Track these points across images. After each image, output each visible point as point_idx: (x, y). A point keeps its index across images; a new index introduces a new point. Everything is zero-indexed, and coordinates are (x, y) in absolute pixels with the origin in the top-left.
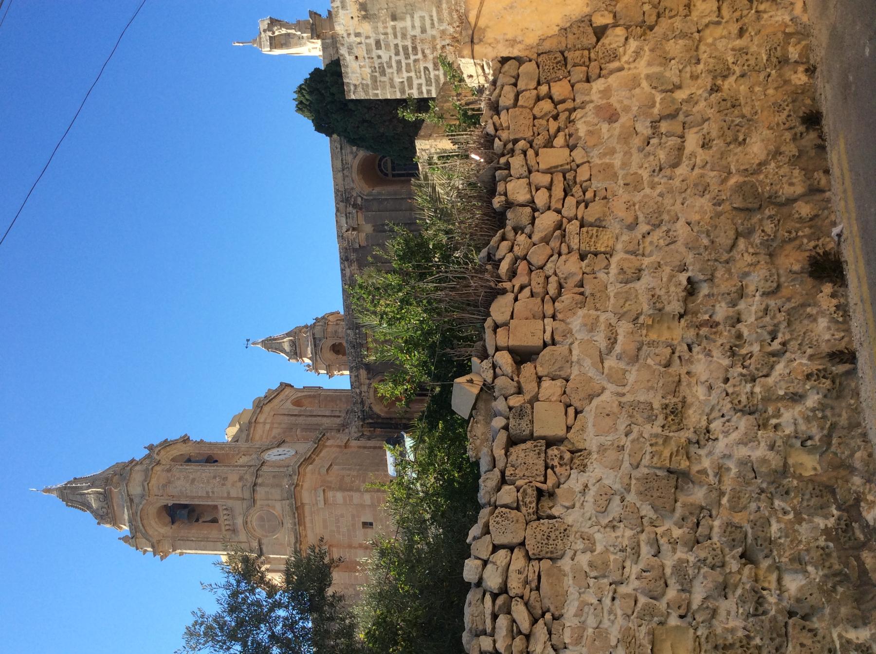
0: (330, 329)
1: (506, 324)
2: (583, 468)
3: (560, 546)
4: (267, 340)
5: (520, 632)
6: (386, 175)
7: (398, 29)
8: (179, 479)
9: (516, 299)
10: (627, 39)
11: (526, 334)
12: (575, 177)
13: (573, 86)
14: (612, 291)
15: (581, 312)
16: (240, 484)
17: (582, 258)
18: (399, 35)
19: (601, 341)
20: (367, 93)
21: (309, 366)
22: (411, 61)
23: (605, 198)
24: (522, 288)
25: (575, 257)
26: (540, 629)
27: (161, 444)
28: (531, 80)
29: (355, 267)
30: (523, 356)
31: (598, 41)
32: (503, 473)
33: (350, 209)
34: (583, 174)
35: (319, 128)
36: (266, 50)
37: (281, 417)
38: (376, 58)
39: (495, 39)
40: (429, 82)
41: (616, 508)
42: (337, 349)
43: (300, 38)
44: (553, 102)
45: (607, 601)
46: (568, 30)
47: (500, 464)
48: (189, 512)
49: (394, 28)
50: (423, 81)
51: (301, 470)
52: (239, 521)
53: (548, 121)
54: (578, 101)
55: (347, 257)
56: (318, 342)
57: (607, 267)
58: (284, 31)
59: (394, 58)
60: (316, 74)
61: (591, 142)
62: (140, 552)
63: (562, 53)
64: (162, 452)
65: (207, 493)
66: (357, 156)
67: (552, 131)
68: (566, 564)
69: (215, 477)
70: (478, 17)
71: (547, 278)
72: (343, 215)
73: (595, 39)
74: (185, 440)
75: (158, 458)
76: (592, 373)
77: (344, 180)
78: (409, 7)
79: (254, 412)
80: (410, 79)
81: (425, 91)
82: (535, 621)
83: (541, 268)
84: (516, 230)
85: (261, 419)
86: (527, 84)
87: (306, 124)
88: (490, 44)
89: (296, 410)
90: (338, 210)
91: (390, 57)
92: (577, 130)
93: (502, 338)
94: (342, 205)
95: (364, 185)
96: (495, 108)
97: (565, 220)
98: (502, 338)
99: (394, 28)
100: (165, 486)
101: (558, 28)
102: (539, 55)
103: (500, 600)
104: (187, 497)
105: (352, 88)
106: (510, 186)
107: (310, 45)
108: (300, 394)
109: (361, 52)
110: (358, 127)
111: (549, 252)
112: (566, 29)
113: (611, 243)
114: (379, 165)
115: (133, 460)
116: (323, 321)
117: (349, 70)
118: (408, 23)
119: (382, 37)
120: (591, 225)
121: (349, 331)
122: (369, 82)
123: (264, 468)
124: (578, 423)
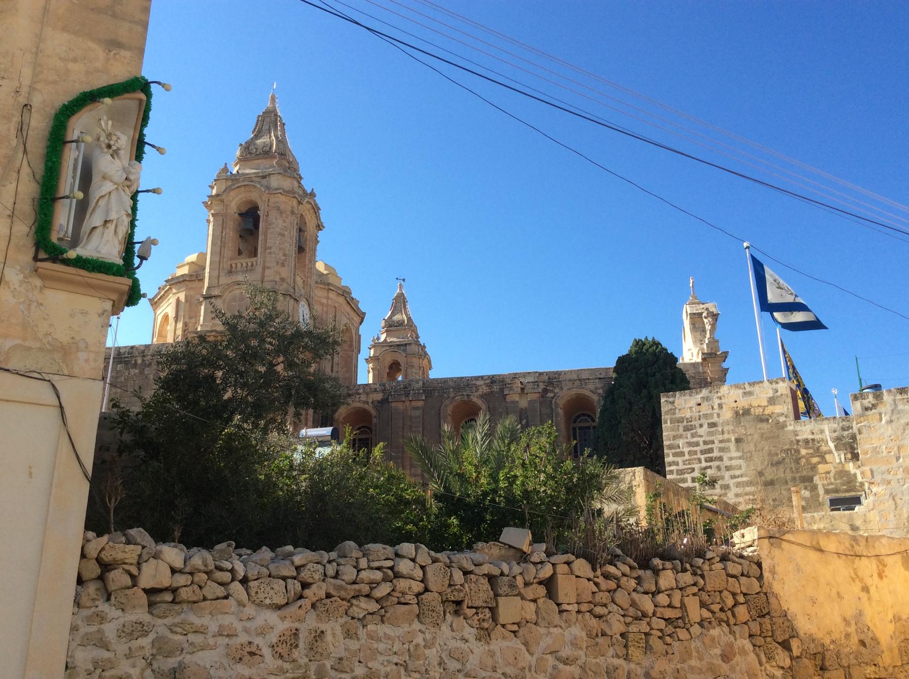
0: (415, 361)
1: (572, 573)
2: (479, 639)
3: (428, 620)
4: (404, 298)
5: (372, 589)
6: (575, 422)
7: (727, 444)
8: (284, 221)
9: (589, 580)
10: (782, 668)
11: (566, 588)
12: (680, 627)
13: (745, 623)
14: (600, 660)
15: (584, 634)
16: (277, 279)
17: (623, 635)
18: (722, 445)
19: (566, 652)
20: (667, 413)
21: (378, 338)
22: (699, 455)
23: (667, 653)
24: (596, 584)
25: (623, 629)
26: (373, 606)
27: (316, 204)
28: (748, 588)
29: (485, 389)
30: (549, 584)
31: (779, 643)
32: (471, 572)
33: (542, 386)
34: (682, 634)
35: (621, 360)
36: (687, 309)
38: (700, 422)
40: (681, 472)
41: (453, 665)
42: (395, 367)
43: (701, 342)
45: (395, 659)
47: (477, 570)
48: (250, 230)
49: (729, 441)
50: (681, 467)
52: (240, 278)
54: (735, 628)
57: (618, 656)
58: (708, 327)
59: (701, 440)
60: (671, 360)
61: (707, 641)
62: (211, 181)
63: (768, 613)
65: (270, 248)
66: (594, 394)
67: (713, 607)
68: (417, 625)
69: (285, 255)
70: (789, 541)
71: (605, 605)
73: (780, 641)
74: (319, 227)
76: (543, 645)
78: (749, 455)
80: (682, 454)
81: (672, 468)
82: (377, 601)
83: (613, 601)
84: (639, 579)
85: (332, 295)
87: (624, 349)
90: (541, 374)
91: (701, 436)
92: (714, 628)
93: (562, 569)
94: (546, 378)
96: (724, 558)
98: (562, 569)
99: (729, 441)
100: (278, 209)
103: (390, 572)
104: (267, 229)
105: (671, 399)
106: (669, 573)
107: (695, 351)
108: (353, 332)
109: (705, 409)
110: (625, 398)
113: (634, 659)
114: (584, 415)
115: (301, 178)
116: (422, 354)
117: (687, 397)
118: (735, 454)
119: (720, 429)
120: (647, 642)
121: (421, 383)
122: (678, 415)
123: (292, 301)
124: (507, 634)
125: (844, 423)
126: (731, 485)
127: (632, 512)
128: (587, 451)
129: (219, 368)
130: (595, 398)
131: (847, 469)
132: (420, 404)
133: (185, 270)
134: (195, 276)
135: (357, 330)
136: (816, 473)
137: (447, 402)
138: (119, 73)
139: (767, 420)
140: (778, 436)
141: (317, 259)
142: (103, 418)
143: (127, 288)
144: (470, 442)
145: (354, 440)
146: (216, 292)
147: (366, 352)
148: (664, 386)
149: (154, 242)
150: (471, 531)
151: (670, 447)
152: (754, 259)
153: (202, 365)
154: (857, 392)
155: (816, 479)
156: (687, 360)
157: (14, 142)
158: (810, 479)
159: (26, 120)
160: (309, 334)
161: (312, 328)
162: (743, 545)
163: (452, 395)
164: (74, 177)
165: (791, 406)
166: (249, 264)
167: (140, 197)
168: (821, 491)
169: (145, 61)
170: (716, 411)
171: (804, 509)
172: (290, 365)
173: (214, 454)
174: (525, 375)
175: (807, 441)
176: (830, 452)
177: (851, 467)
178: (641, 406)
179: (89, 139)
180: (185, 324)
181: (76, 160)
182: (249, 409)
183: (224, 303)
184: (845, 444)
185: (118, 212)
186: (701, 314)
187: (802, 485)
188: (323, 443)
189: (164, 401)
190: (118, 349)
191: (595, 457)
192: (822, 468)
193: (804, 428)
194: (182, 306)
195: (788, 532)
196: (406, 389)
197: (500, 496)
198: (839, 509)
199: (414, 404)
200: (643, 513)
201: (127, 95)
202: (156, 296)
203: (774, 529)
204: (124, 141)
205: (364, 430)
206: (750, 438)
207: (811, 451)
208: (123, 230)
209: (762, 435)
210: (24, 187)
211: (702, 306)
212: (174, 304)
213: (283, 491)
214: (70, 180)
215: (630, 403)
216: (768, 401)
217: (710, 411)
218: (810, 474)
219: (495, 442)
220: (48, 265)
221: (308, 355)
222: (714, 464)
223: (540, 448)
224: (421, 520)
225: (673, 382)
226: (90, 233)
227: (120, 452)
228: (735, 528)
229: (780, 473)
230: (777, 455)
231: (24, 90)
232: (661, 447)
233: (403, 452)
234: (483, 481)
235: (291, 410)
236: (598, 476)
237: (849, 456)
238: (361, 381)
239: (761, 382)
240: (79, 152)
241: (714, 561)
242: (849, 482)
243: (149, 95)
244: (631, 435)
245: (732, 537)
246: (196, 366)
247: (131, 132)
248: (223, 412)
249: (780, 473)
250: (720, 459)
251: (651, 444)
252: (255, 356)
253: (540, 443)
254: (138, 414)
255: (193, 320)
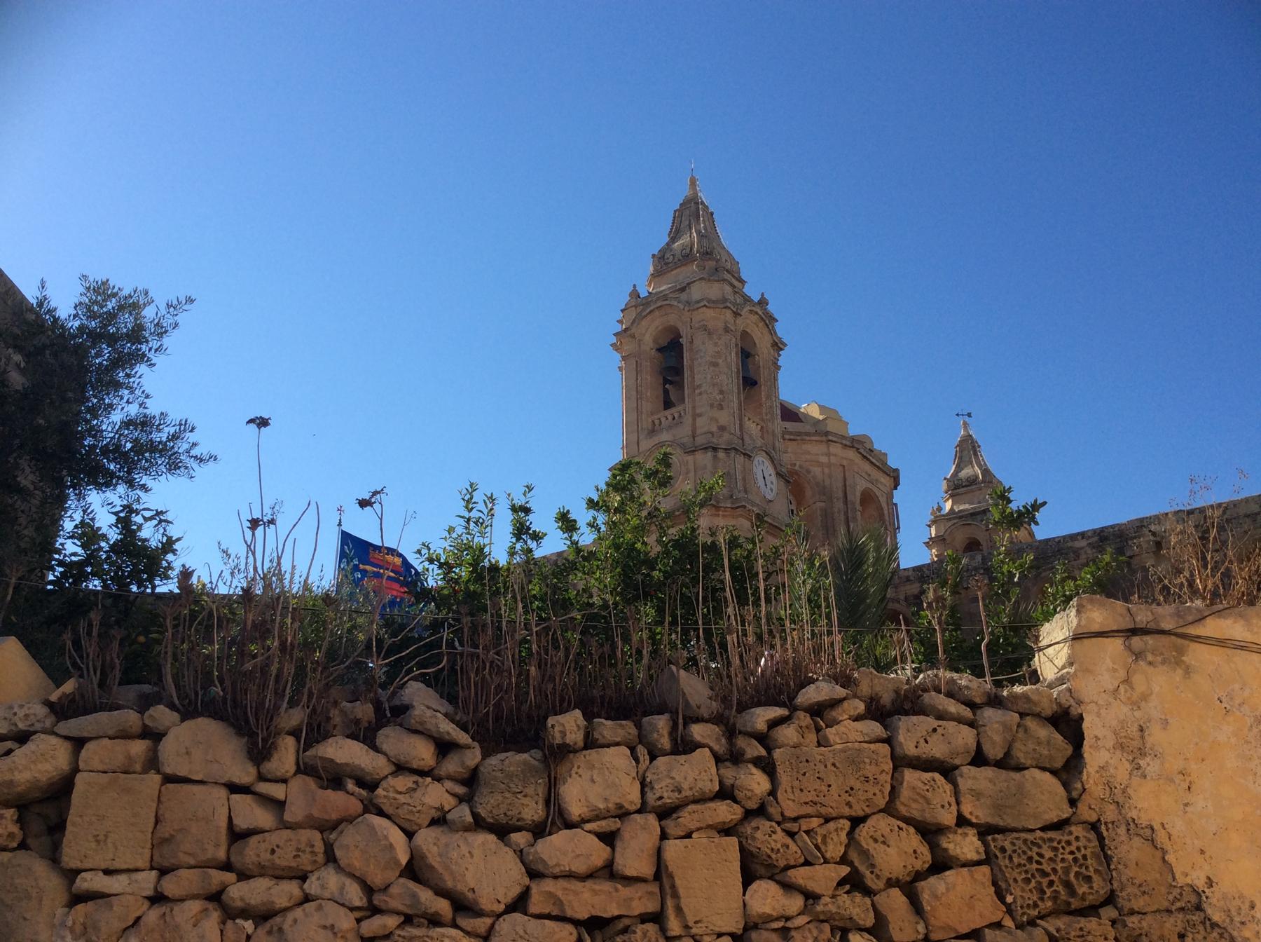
1: (152, 763)
8: (716, 344)
9: (234, 788)
11: (110, 825)
16: (714, 429)
21: (940, 509)
28: (998, 808)
39: (1145, 697)
42: (972, 546)
44: (919, 876)
46: (1197, 917)
51: (739, 511)
53: (844, 860)
56: (979, 517)
63: (1110, 899)
64: (754, 318)
65: (699, 386)
69: (721, 392)
70: (1221, 643)
74: (778, 346)
75: (745, 311)
77: (1247, 516)
79: (844, 437)
86: (977, 795)
88: (1126, 681)
89: (855, 497)
97: (482, 924)
100: (705, 328)
101: (1200, 884)
102: (1094, 827)
106: (618, 758)
111: (377, 879)
112: (1199, 908)
115: (743, 282)
123: (740, 459)
135: (890, 497)
166: (676, 415)
241: (842, 713)
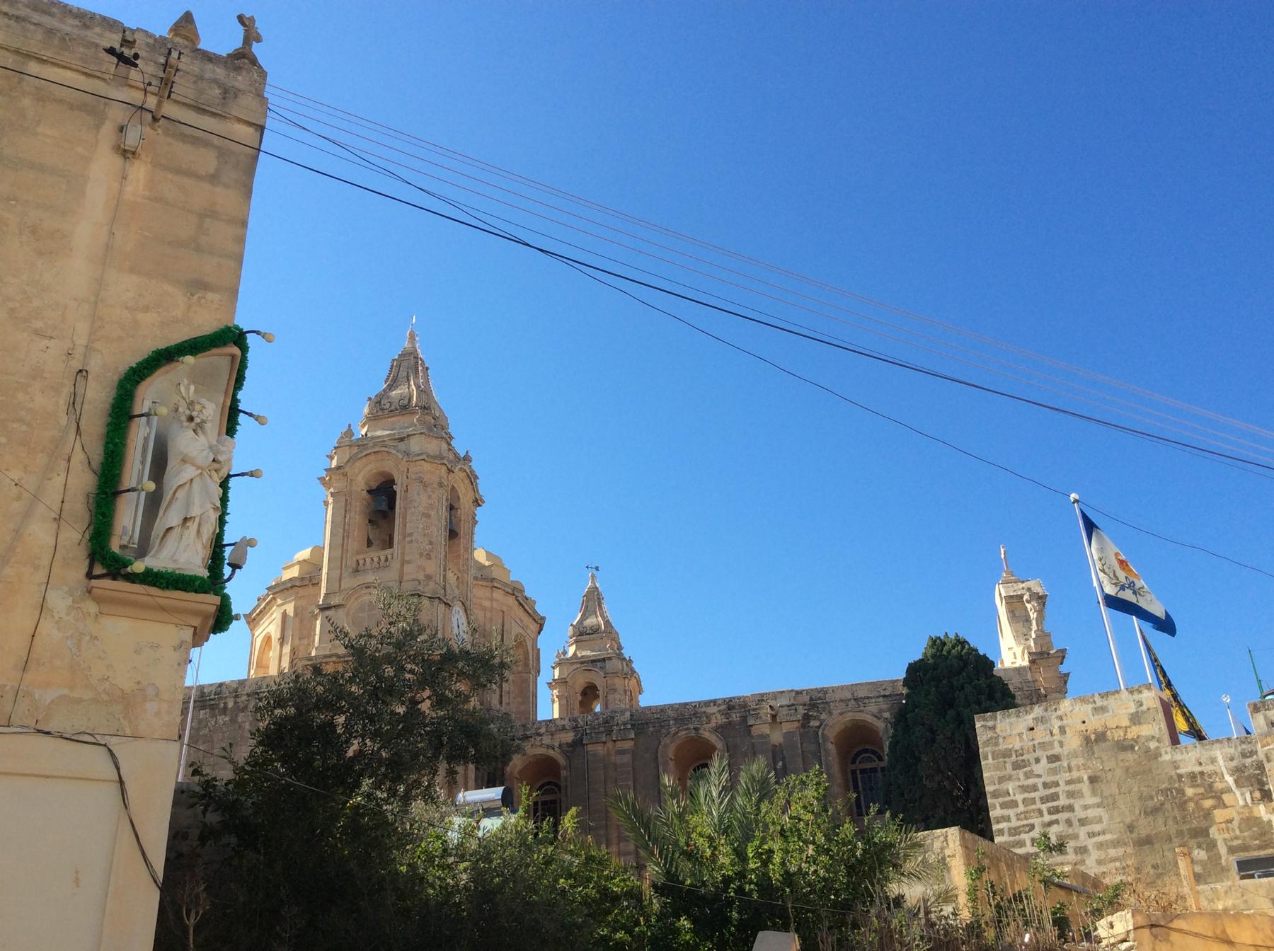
0: (618, 682)
6: (853, 762)
8: (430, 497)
16: (421, 577)
20: (987, 743)
21: (565, 653)
22: (1039, 805)
29: (721, 720)
33: (801, 710)
35: (913, 669)
36: (1001, 591)
37: (500, 621)
38: (1035, 755)
40: (1014, 831)
42: (590, 693)
49: (1080, 780)
52: (370, 578)
55: (733, 707)
58: (1033, 615)
59: (1039, 782)
60: (985, 665)
62: (329, 449)
65: (411, 535)
66: (878, 718)
69: (431, 543)
72: (792, 701)
74: (477, 502)
75: (456, 470)
77: (841, 701)
79: (506, 585)
80: (1013, 804)
85: (498, 595)
90: (799, 693)
91: (1039, 776)
94: (806, 699)
95: (837, 729)
99: (1080, 780)
105: (990, 724)
107: (1018, 650)
108: (529, 644)
109: (1040, 735)
110: (923, 724)
114: (866, 751)
115: (451, 438)
117: (1013, 719)
121: (628, 714)
122: (1002, 747)
125: (1244, 746)
126: (1090, 848)
127: (947, 896)
128: (873, 809)
129: (340, 711)
130: (880, 725)
131: (1256, 814)
132: (628, 745)
133: (294, 572)
134: (308, 579)
135: (535, 641)
136: (1212, 822)
137: (666, 741)
138: (205, 323)
139: (1132, 747)
140: (1150, 771)
141: (475, 545)
142: (180, 792)
143: (213, 609)
144: (702, 800)
145: (536, 804)
146: (335, 600)
147: (549, 672)
148: (979, 704)
149: (251, 543)
150: (711, 938)
151: (996, 795)
152: (1085, 517)
153: (317, 707)
154: (1257, 700)
155: (1213, 832)
156: (1007, 664)
157: (64, 421)
158: (1204, 832)
159: (80, 391)
160: (465, 654)
161: (469, 647)
162: (1112, 940)
163: (673, 730)
164: (143, 463)
165: (1163, 725)
167: (233, 483)
168: (1223, 850)
169: (238, 304)
170: (1057, 737)
171: (1198, 878)
172: (440, 701)
173: (334, 838)
174: (776, 695)
175: (1193, 776)
176: (1229, 790)
177: (1262, 811)
178: (949, 734)
179: (163, 411)
180: (293, 652)
181: (146, 439)
182: (383, 769)
183: (347, 614)
184: (1249, 778)
185: (203, 506)
186: (1021, 596)
187: (1193, 843)
188: (490, 812)
189: (264, 763)
190: (201, 688)
191: (888, 814)
192: (1219, 815)
193: (1185, 756)
194: (290, 623)
195: (1177, 916)
196: (607, 724)
197: (751, 882)
198: (1252, 876)
199: (620, 745)
200: (963, 899)
201: (214, 351)
202: (254, 610)
203: (1157, 914)
204: (211, 411)
205: (550, 789)
206: (1109, 775)
207: (1201, 790)
208: (210, 528)
209: (1127, 769)
210: (81, 480)
211: (1021, 585)
212: (279, 621)
213: (434, 888)
214: (138, 466)
215: (932, 731)
216: (1131, 720)
217: (1048, 738)
218: (1204, 824)
219: (739, 799)
220: (107, 583)
221: (462, 687)
222: (1062, 816)
223: (805, 807)
224: (637, 923)
225: (991, 697)
226: (164, 536)
227: (203, 839)
228: (1097, 913)
229: (1161, 825)
230: (1152, 798)
231: (78, 352)
232: (982, 794)
233: (607, 818)
234: (724, 860)
235: (443, 767)
236: (891, 845)
237: (1257, 794)
238: (542, 716)
239: (1118, 692)
240: (150, 428)
242: (1263, 834)
243: (244, 349)
244: (938, 778)
245: (1096, 929)
246: (308, 711)
247: (221, 399)
248: (347, 776)
249: (1161, 825)
250: (1070, 808)
251: (967, 791)
252: (390, 691)
253: (803, 799)
254: (229, 782)
255: (305, 642)
